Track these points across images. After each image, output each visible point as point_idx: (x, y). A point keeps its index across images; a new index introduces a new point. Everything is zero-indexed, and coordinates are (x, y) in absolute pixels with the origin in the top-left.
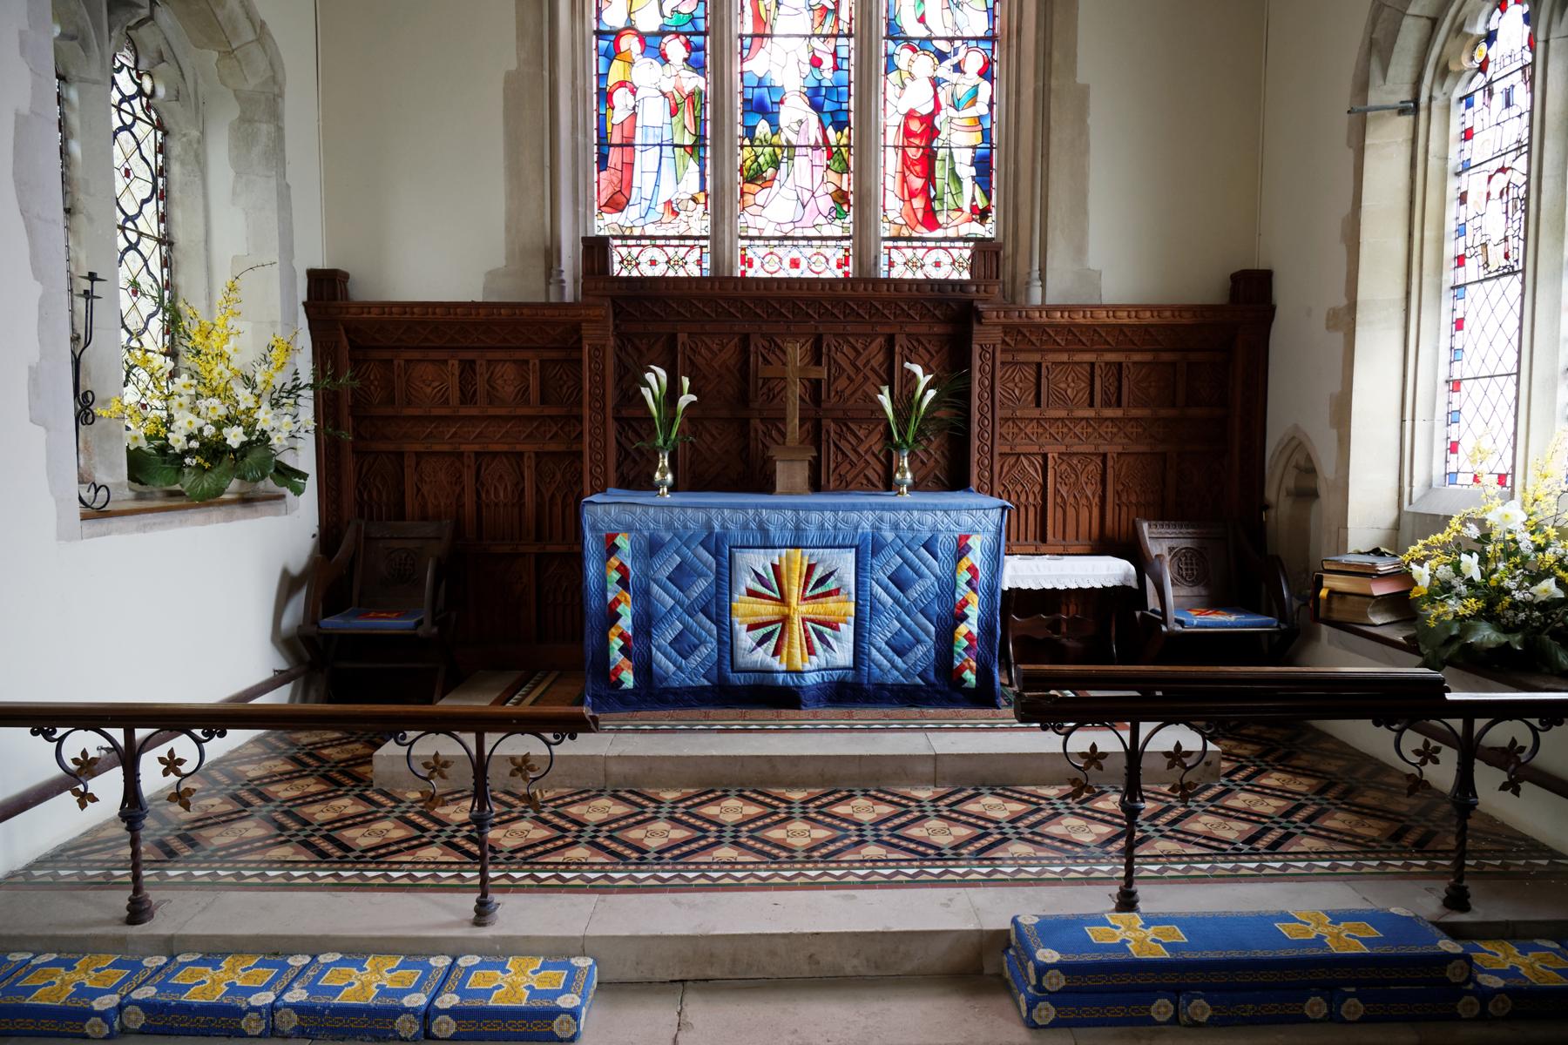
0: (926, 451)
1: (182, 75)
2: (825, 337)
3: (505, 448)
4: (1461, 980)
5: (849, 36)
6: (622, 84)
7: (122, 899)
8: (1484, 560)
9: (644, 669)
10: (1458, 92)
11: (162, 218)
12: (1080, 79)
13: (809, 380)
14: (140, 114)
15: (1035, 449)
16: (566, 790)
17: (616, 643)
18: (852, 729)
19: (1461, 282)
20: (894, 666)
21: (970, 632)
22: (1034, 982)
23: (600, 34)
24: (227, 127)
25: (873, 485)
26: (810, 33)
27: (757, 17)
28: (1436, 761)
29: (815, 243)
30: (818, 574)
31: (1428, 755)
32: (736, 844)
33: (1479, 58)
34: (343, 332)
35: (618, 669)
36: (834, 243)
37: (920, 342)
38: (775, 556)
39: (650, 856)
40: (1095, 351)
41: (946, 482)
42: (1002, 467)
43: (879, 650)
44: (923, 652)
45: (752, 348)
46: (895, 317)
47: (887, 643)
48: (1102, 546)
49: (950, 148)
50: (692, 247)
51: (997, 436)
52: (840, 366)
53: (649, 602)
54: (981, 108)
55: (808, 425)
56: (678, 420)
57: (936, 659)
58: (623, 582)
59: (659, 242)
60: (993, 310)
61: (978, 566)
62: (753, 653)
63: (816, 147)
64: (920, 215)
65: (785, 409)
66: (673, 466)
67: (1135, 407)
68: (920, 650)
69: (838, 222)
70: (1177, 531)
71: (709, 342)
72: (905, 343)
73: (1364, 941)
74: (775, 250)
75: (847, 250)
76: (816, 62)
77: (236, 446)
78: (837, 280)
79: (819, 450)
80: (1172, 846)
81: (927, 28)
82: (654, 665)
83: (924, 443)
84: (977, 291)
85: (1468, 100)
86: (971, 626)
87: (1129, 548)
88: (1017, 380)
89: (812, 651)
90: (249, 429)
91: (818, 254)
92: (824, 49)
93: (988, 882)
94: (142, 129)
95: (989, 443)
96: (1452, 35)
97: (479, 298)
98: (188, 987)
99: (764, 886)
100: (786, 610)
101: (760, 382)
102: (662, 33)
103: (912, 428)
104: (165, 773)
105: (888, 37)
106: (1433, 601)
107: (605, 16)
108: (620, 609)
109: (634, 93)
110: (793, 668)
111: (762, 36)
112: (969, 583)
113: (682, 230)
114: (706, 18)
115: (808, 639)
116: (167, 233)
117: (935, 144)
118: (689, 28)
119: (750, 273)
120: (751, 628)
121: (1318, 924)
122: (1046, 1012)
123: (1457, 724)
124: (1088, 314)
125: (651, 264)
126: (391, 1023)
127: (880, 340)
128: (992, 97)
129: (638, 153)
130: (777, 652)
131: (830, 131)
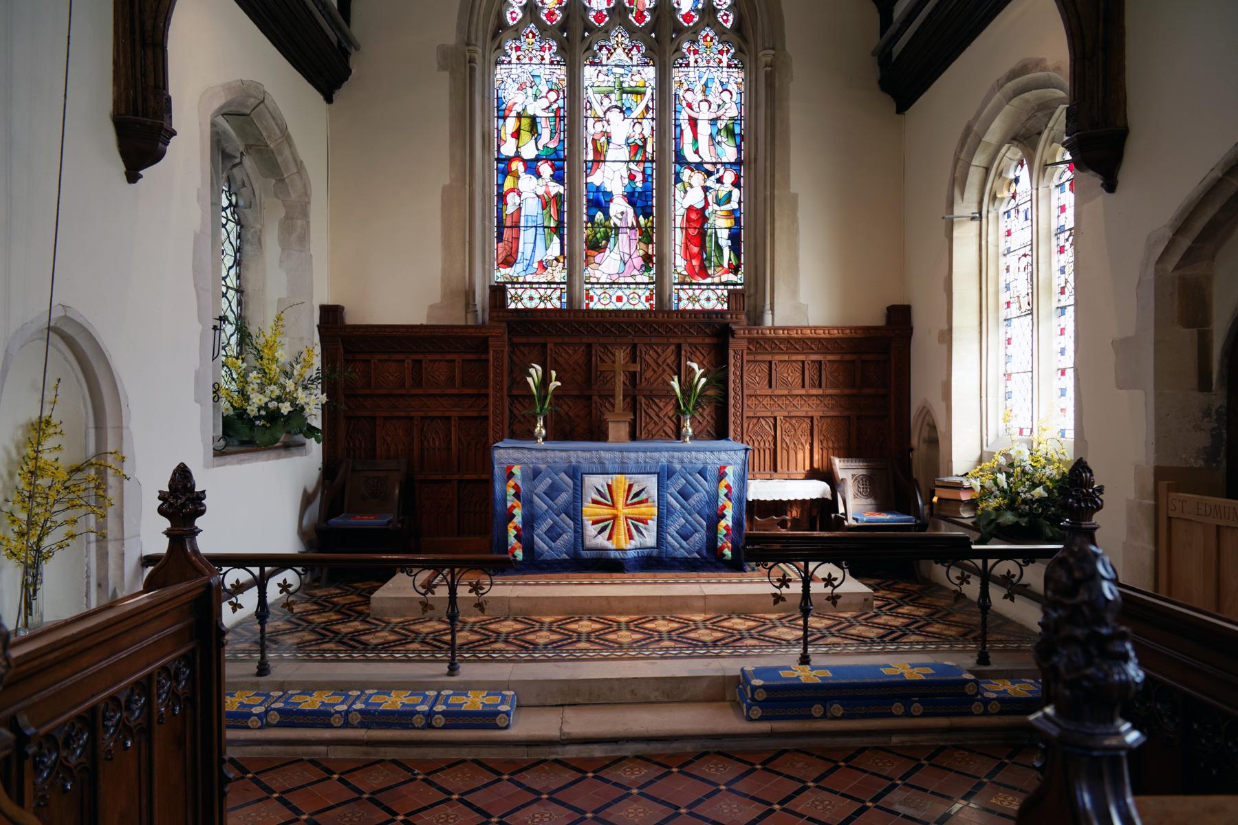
0: (701, 415)
1: (254, 194)
2: (638, 345)
3: (440, 414)
4: (973, 693)
5: (652, 161)
6: (512, 190)
7: (253, 668)
8: (1009, 475)
9: (529, 547)
10: (1003, 209)
11: (238, 277)
13: (629, 372)
14: (231, 218)
15: (769, 414)
16: (486, 617)
17: (512, 533)
18: (656, 583)
19: (1009, 317)
20: (682, 547)
21: (727, 525)
22: (750, 696)
23: (499, 160)
24: (277, 225)
25: (669, 436)
26: (628, 159)
27: (595, 150)
28: (968, 583)
29: (632, 286)
30: (635, 490)
31: (963, 579)
32: (589, 641)
33: (1012, 191)
34: (340, 343)
35: (514, 549)
36: (644, 286)
37: (697, 348)
38: (608, 479)
40: (804, 354)
41: (714, 434)
42: (749, 425)
43: (672, 536)
44: (699, 537)
45: (594, 352)
46: (682, 333)
47: (677, 532)
48: (812, 474)
49: (715, 229)
50: (555, 289)
51: (745, 406)
52: (648, 363)
53: (532, 507)
54: (734, 205)
55: (628, 400)
56: (549, 397)
57: (707, 542)
58: (517, 495)
59: (534, 286)
60: (741, 329)
61: (731, 485)
62: (595, 538)
63: (632, 228)
64: (697, 270)
65: (614, 390)
66: (545, 426)
67: (830, 388)
68: (697, 536)
69: (646, 274)
70: (857, 464)
71: (567, 348)
72: (688, 349)
73: (924, 675)
74: (607, 291)
75: (652, 291)
76: (632, 177)
77: (285, 414)
78: (647, 311)
79: (635, 415)
81: (700, 157)
82: (535, 547)
83: (700, 410)
84: (731, 318)
85: (1007, 213)
87: (827, 475)
88: (757, 371)
89: (631, 537)
90: (293, 402)
91: (634, 293)
94: (231, 226)
95: (740, 410)
96: (997, 177)
97: (425, 323)
98: (300, 703)
99: (606, 659)
100: (614, 512)
101: (599, 373)
102: (538, 159)
103: (692, 402)
104: (281, 592)
105: (676, 162)
106: (982, 500)
107: (502, 150)
108: (515, 512)
109: (520, 196)
110: (620, 548)
111: (599, 162)
112: (726, 495)
113: (549, 278)
114: (564, 151)
115: (629, 530)
116: (240, 286)
117: (705, 227)
118: (554, 156)
119: (591, 305)
120: (595, 523)
121: (904, 668)
122: (757, 712)
123: (979, 562)
124: (799, 332)
126: (411, 719)
127: (673, 347)
128: (740, 198)
129: (522, 232)
130: (610, 538)
131: (641, 218)
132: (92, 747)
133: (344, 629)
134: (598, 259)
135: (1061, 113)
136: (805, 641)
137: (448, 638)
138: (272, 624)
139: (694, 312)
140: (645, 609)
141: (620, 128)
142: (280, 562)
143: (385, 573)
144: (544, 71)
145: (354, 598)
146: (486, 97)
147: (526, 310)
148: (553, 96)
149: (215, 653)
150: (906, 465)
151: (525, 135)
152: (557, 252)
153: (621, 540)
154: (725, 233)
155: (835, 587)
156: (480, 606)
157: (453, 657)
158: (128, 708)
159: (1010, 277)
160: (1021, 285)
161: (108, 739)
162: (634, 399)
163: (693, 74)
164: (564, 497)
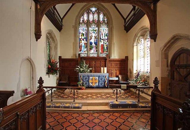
7: (51, 100)
31: (136, 91)
58: (82, 79)
62: (91, 84)
76: (95, 41)
86: (106, 82)
92: (95, 40)
97: (71, 58)
99: (92, 100)
102: (84, 39)
122: (111, 107)
132: (28, 116)
133: (61, 95)
135: (148, 32)
138: (53, 94)
140: (96, 94)
141: (94, 35)
142: (53, 88)
143: (66, 89)
144: (85, 28)
146: (78, 31)
148: (86, 31)
151: (82, 36)
158: (33, 109)
161: (31, 113)
163: (102, 28)
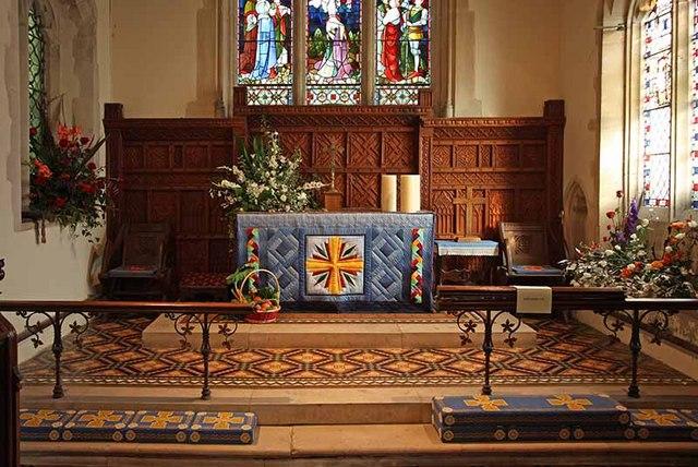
6: (250, 13)
7: (50, 391)
10: (644, 20)
11: (42, 81)
12: (470, 9)
31: (618, 326)
32: (311, 370)
39: (274, 375)
44: (397, 285)
62: (315, 286)
80: (511, 373)
85: (648, 23)
86: (419, 273)
87: (491, 234)
89: (344, 286)
93: (425, 385)
99: (325, 386)
122: (450, 435)
123: (631, 312)
125: (262, 98)
130: (327, 286)
133: (120, 357)
134: (316, 66)
136: (487, 371)
137: (202, 367)
139: (391, 106)
140: (355, 345)
145: (130, 332)
147: (261, 106)
149: (11, 397)
150: (557, 224)
152: (285, 61)
153: (336, 288)
154: (416, 44)
155: (512, 332)
156: (226, 344)
157: (206, 383)
159: (649, 76)
160: (661, 82)
162: (345, 176)
164: (291, 254)
